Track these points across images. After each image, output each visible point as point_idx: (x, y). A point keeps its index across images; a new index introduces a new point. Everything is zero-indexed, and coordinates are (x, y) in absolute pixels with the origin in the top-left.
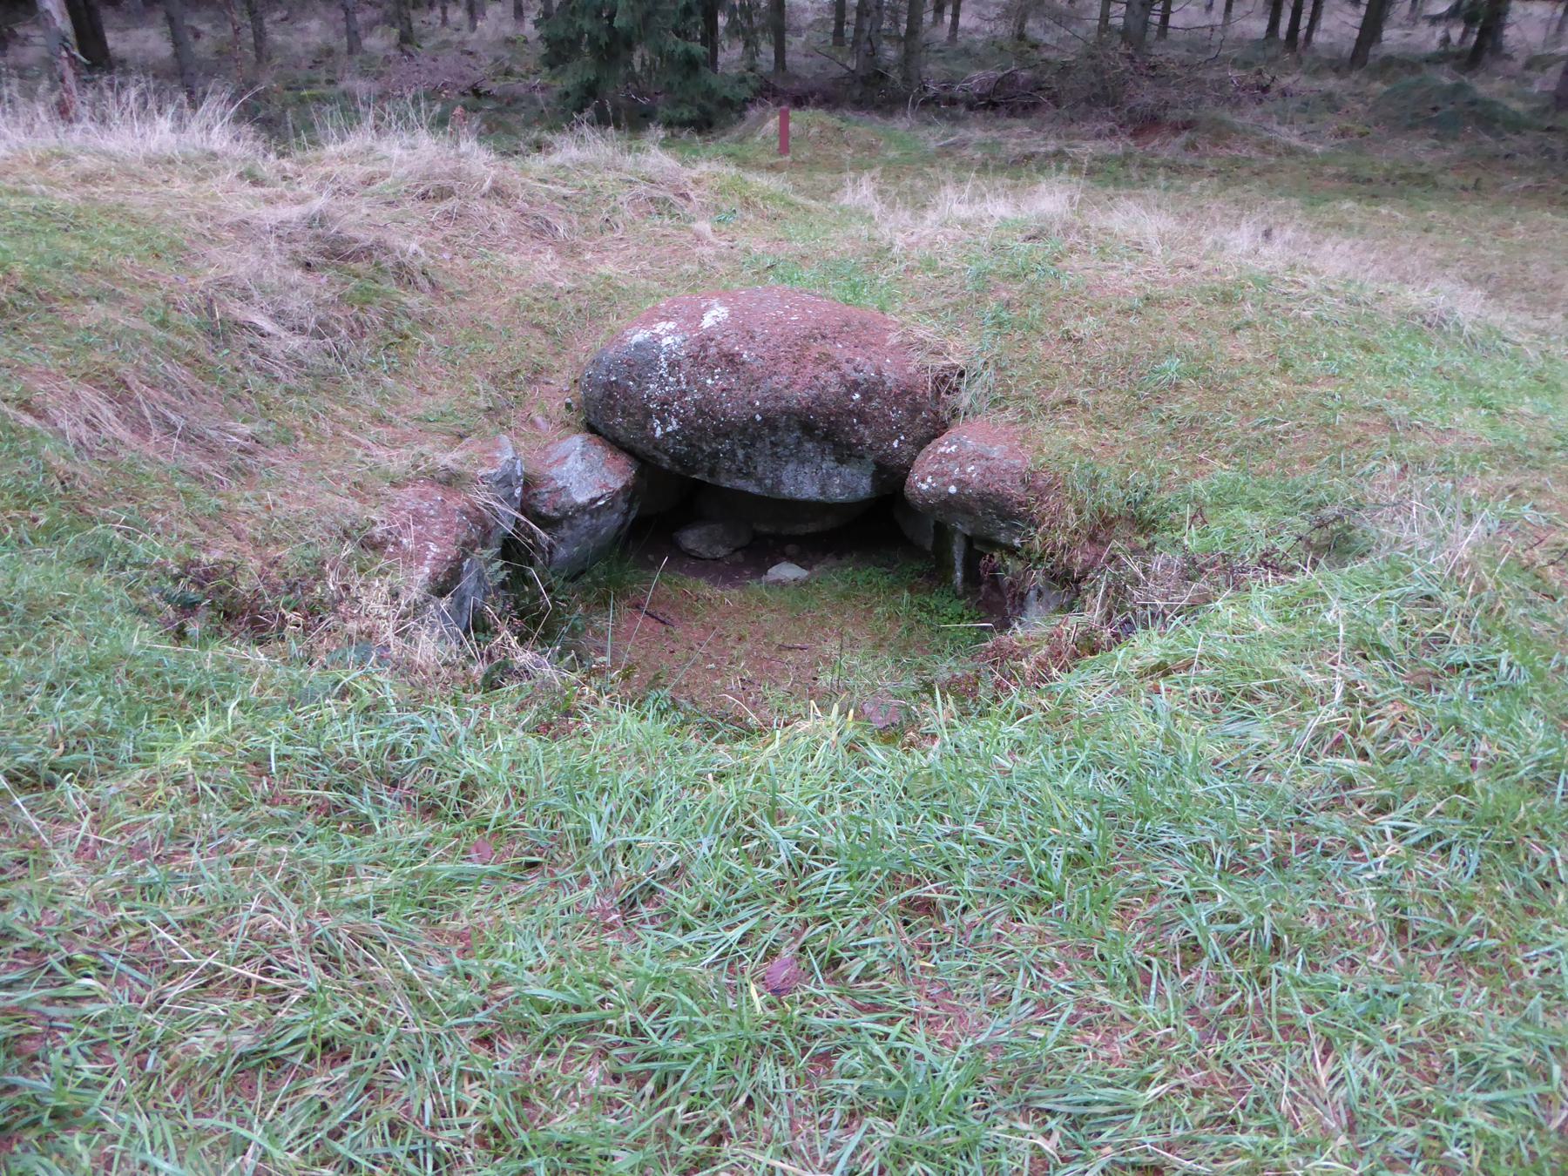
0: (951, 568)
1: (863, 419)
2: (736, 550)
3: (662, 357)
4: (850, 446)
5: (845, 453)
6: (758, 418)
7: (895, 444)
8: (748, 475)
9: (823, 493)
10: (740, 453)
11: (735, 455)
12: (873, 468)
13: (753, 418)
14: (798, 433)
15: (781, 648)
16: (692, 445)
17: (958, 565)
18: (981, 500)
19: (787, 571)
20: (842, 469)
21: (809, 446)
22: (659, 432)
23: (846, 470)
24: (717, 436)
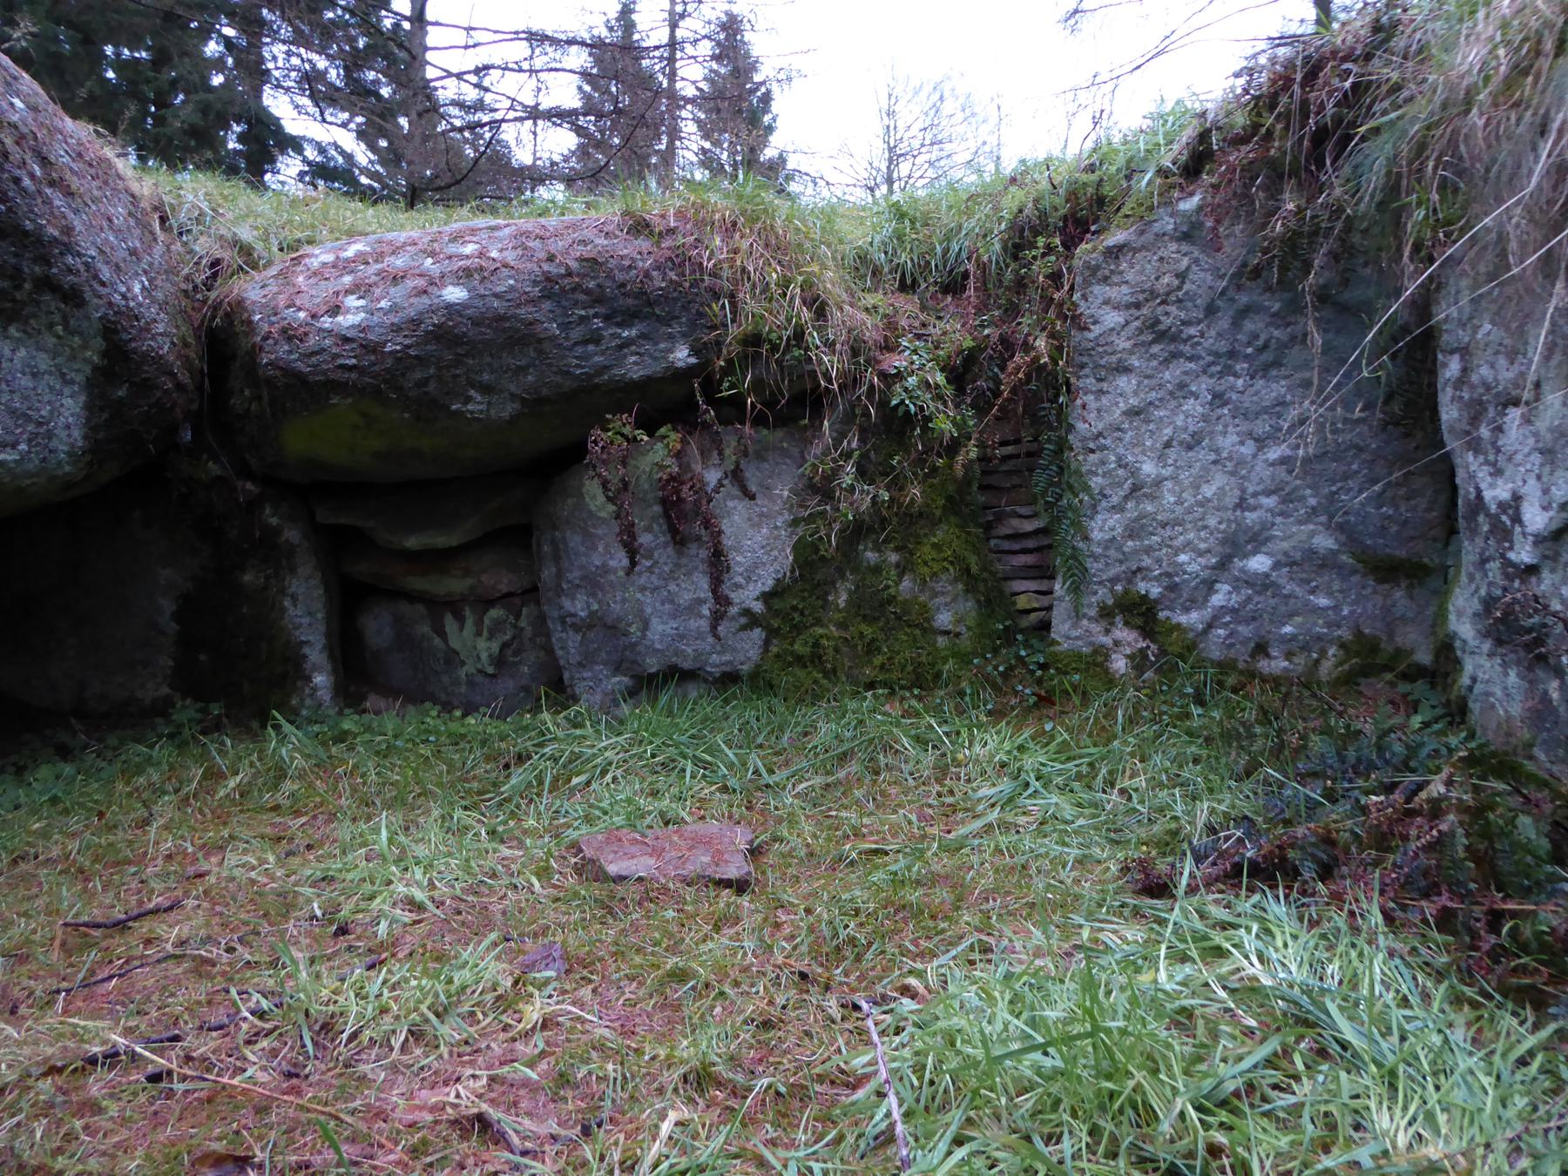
18: (547, 295)
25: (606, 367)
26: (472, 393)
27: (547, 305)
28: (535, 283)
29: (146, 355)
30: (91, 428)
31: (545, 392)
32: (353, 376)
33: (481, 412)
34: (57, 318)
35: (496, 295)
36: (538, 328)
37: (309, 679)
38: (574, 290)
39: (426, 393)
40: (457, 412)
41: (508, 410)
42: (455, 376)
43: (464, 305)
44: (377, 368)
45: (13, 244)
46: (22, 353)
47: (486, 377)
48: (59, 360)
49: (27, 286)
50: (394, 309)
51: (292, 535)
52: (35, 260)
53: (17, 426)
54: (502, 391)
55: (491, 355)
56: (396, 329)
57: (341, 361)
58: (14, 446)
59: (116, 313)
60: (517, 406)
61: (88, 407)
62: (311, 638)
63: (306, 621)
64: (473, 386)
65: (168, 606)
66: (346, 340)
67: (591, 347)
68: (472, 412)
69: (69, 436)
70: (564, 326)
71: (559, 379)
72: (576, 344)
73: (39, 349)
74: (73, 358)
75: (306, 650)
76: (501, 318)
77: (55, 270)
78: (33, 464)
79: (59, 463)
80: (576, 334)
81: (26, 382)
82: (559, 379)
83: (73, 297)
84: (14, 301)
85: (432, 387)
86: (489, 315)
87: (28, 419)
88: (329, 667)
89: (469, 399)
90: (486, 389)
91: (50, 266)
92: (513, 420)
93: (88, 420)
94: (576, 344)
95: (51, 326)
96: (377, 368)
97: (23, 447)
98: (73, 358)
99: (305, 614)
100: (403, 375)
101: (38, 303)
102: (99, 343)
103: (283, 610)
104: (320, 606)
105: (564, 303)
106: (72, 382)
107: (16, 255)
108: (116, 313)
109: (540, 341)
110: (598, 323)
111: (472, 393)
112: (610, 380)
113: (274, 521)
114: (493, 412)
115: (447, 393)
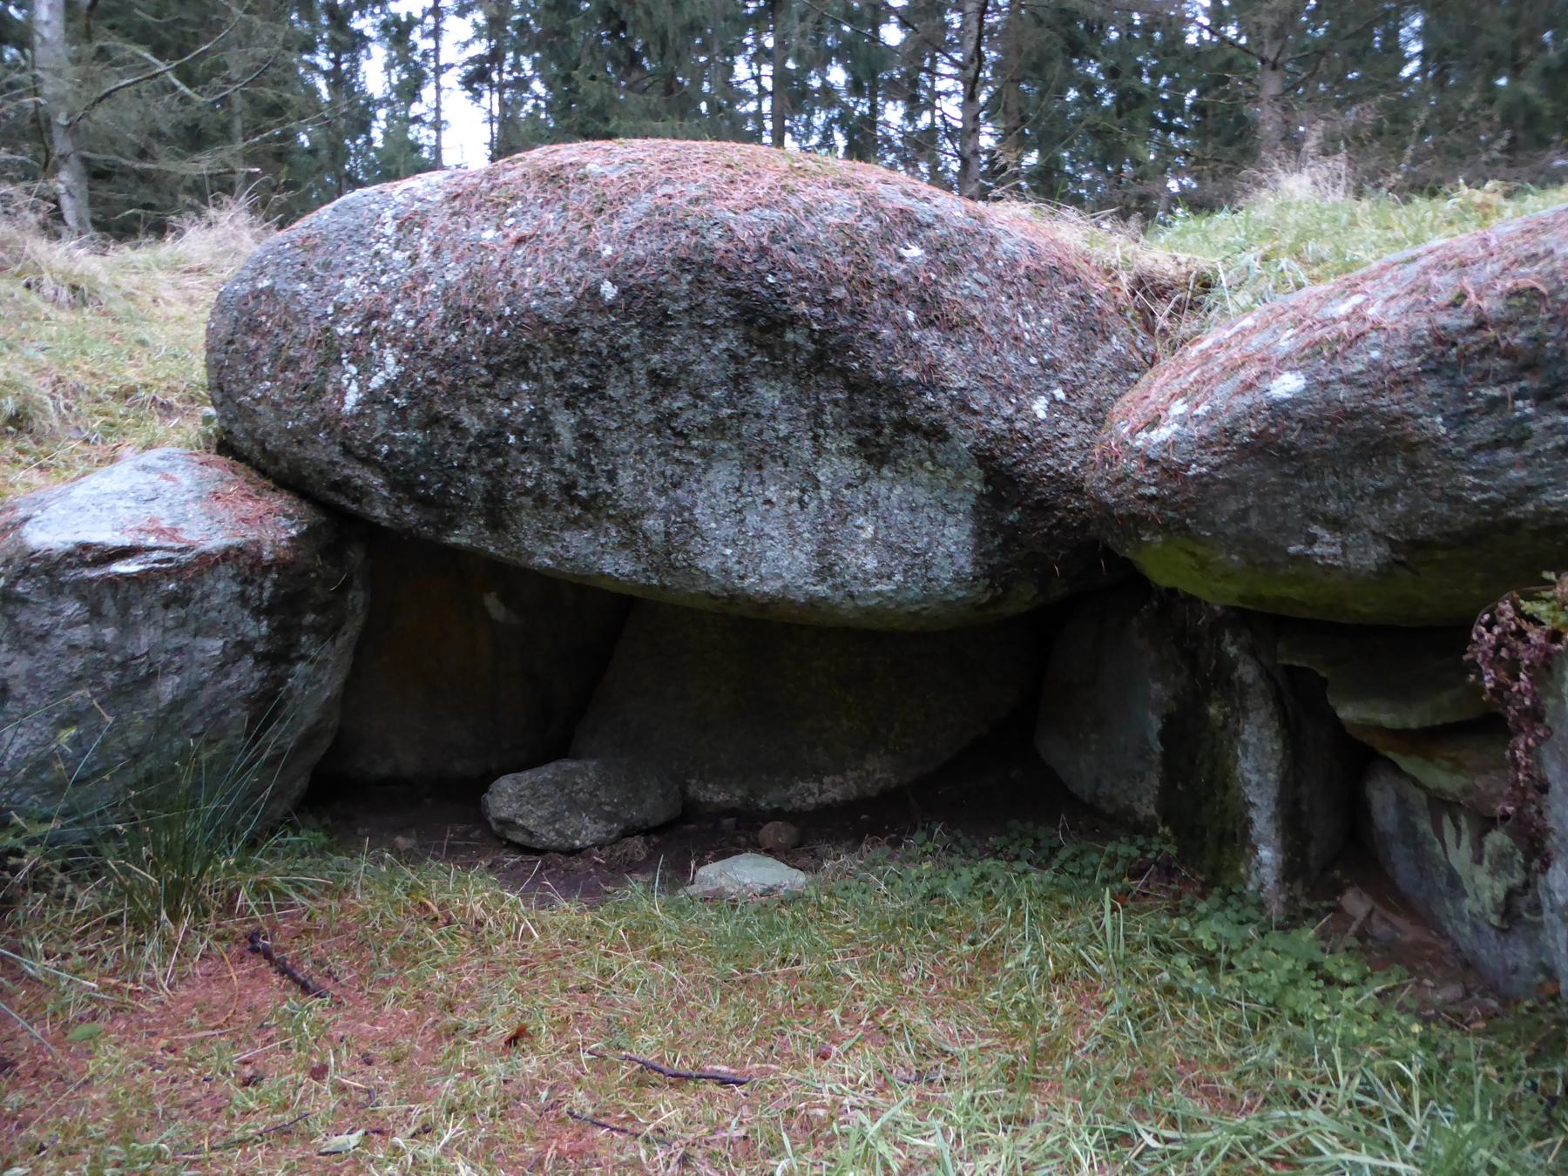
0: (1237, 838)
1: (933, 312)
2: (629, 832)
3: (388, 215)
4: (893, 391)
5: (889, 423)
6: (609, 291)
7: (1040, 407)
8: (593, 509)
9: (825, 572)
10: (564, 422)
11: (550, 435)
12: (974, 481)
13: (594, 293)
14: (729, 340)
15: (649, 1075)
16: (434, 420)
17: (1263, 822)
18: (1436, 367)
19: (750, 873)
20: (879, 488)
21: (769, 395)
22: (352, 396)
23: (891, 490)
24: (497, 371)
25: (1530, 489)
26: (1315, 529)
27: (1431, 385)
28: (1415, 350)
29: (1036, 478)
30: (981, 554)
31: (1421, 530)
32: (1153, 508)
33: (1335, 557)
34: (924, 456)
35: (1347, 380)
36: (1409, 427)
37: (1255, 849)
38: (1483, 353)
39: (1248, 530)
40: (1295, 558)
41: (1372, 556)
42: (1284, 507)
43: (1295, 402)
44: (1178, 498)
45: (869, 396)
46: (898, 490)
47: (1332, 506)
48: (937, 493)
49: (886, 431)
50: (1213, 414)
51: (1247, 671)
52: (890, 406)
53: (893, 559)
54: (1358, 528)
55: (1336, 474)
56: (1205, 443)
57: (1142, 490)
58: (889, 578)
59: (989, 441)
60: (1384, 550)
61: (978, 534)
62: (1257, 801)
63: (1254, 778)
64: (1314, 520)
65: (1156, 724)
66: (1151, 462)
67: (1505, 454)
68: (1322, 557)
69: (952, 564)
70: (1458, 420)
71: (1444, 509)
72: (1478, 448)
73: (916, 485)
74: (951, 489)
75: (1253, 814)
76: (1352, 415)
77: (910, 412)
78: (915, 591)
79: (945, 590)
80: (1483, 430)
81: (903, 517)
82: (1444, 509)
83: (937, 433)
84: (879, 445)
85: (1254, 520)
86: (1331, 413)
87: (905, 551)
88: (1278, 843)
89: (1312, 540)
90: (1335, 524)
91: (905, 408)
92: (1385, 572)
93: (977, 546)
94: (1478, 448)
95: (920, 463)
96: (1178, 498)
97: (898, 577)
98: (951, 489)
99: (1256, 769)
100: (1212, 506)
101: (902, 444)
102: (977, 472)
103: (1236, 758)
104: (1273, 764)
105: (1463, 378)
106: (956, 512)
107: (872, 405)
108: (989, 441)
109: (1412, 448)
110: (1525, 407)
111: (1315, 529)
112: (1540, 513)
113: (1233, 651)
114: (1351, 558)
115: (1278, 531)
